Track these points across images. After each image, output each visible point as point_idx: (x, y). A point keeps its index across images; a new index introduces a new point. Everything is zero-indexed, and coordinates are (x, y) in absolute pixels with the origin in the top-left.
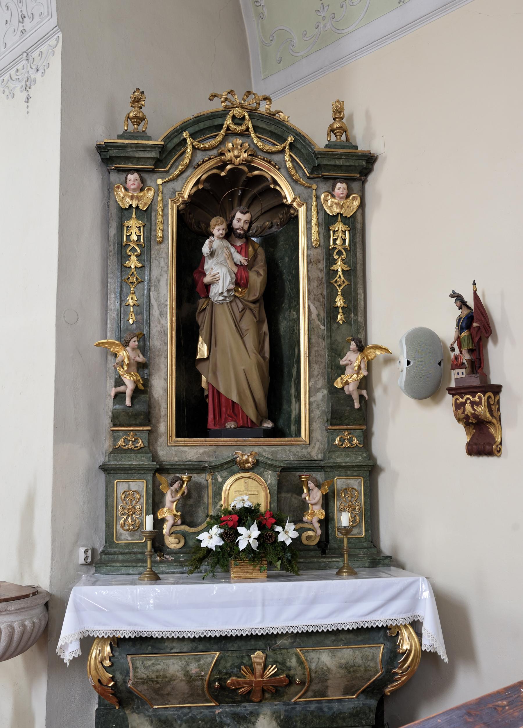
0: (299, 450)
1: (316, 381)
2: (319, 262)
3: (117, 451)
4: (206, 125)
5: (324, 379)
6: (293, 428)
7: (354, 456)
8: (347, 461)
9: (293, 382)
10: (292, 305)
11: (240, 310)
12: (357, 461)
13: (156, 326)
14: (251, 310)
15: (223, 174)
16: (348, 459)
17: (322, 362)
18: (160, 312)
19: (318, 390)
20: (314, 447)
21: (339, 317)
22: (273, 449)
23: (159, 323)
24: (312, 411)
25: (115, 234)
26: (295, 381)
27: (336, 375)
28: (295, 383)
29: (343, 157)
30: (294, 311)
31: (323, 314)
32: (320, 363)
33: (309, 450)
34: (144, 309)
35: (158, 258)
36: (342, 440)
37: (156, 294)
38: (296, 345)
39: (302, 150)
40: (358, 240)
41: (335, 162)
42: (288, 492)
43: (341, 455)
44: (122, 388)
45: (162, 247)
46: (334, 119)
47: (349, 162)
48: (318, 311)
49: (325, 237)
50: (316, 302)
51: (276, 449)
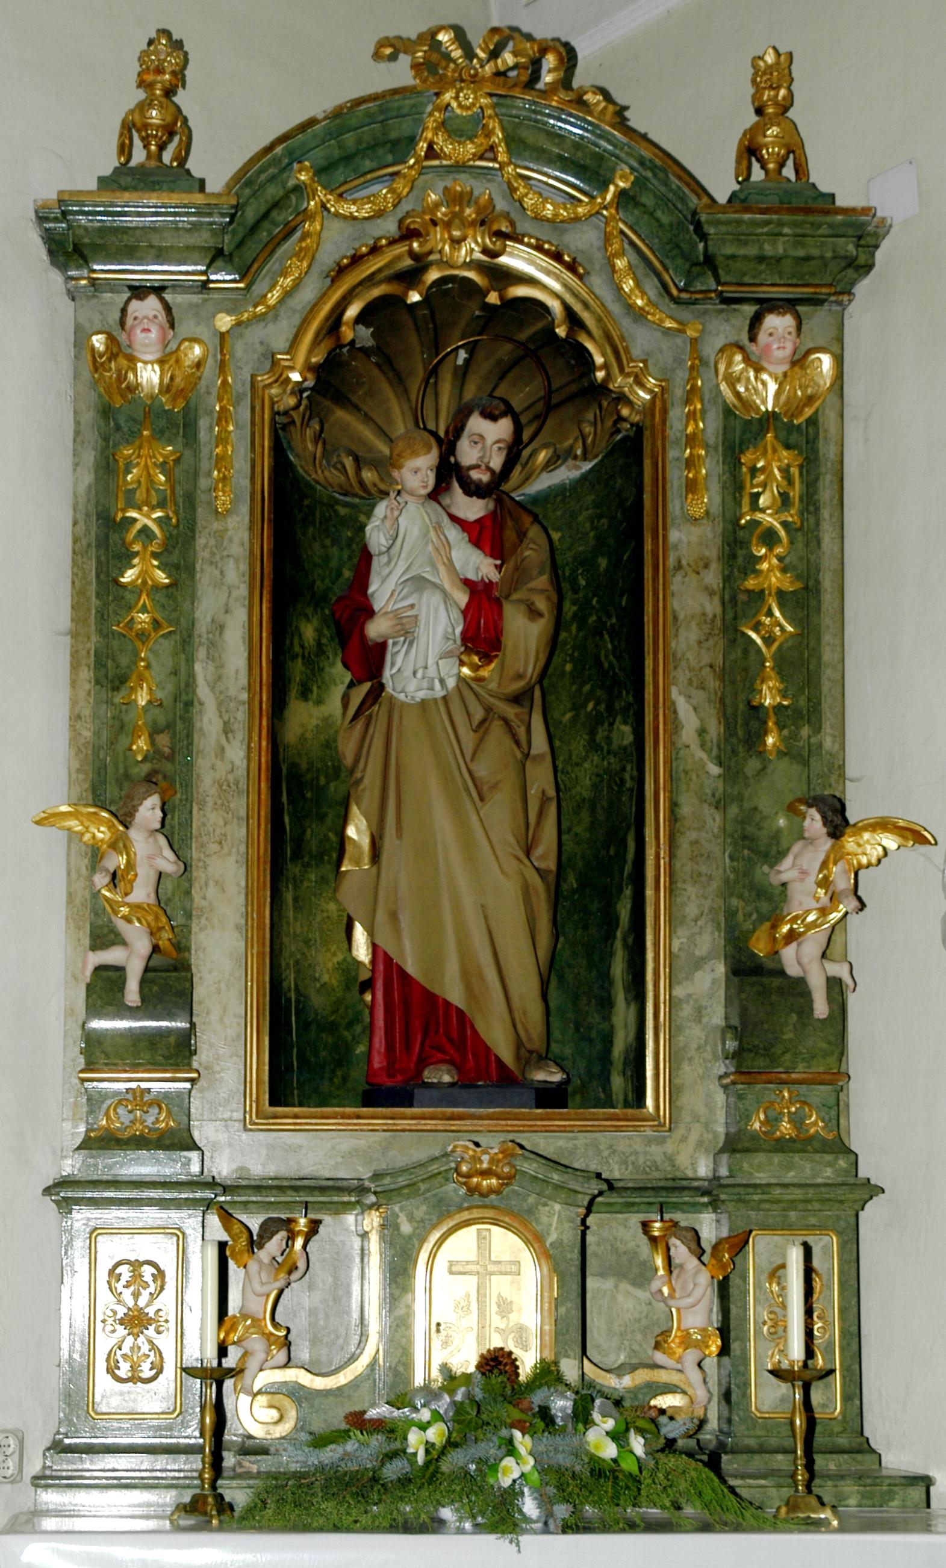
0: (639, 1147)
1: (693, 935)
2: (706, 566)
3: (100, 1142)
4: (359, 140)
5: (718, 928)
6: (617, 1082)
7: (808, 1166)
8: (786, 1181)
9: (618, 944)
10: (617, 706)
11: (475, 723)
12: (819, 1181)
13: (213, 767)
14: (505, 720)
15: (415, 297)
16: (792, 1174)
17: (710, 878)
18: (225, 723)
19: (698, 964)
20: (684, 1139)
21: (770, 740)
22: (561, 1143)
23: (222, 759)
24: (680, 1029)
25: (89, 488)
26: (624, 939)
27: (755, 916)
28: (625, 945)
29: (786, 230)
30: (625, 723)
31: (715, 729)
32: (704, 879)
33: (670, 1147)
34: (178, 717)
35: (218, 557)
36: (772, 1121)
37: (211, 668)
38: (629, 827)
39: (659, 214)
40: (825, 494)
41: (761, 248)
42: (602, 1275)
43: (771, 1163)
44: (112, 956)
45: (230, 526)
46: (759, 111)
47: (803, 245)
48: (701, 720)
49: (724, 488)
50: (694, 692)
51: (570, 1145)
